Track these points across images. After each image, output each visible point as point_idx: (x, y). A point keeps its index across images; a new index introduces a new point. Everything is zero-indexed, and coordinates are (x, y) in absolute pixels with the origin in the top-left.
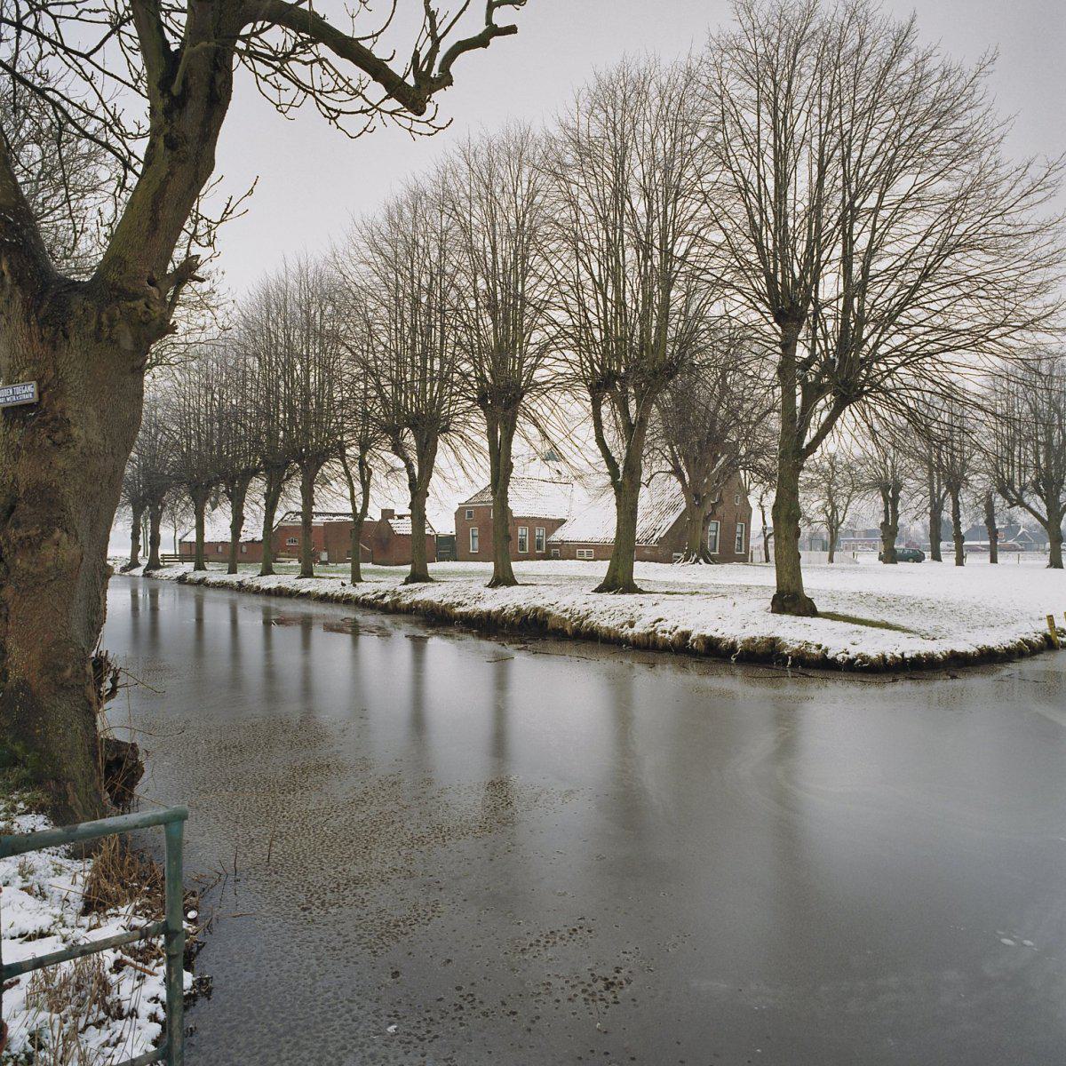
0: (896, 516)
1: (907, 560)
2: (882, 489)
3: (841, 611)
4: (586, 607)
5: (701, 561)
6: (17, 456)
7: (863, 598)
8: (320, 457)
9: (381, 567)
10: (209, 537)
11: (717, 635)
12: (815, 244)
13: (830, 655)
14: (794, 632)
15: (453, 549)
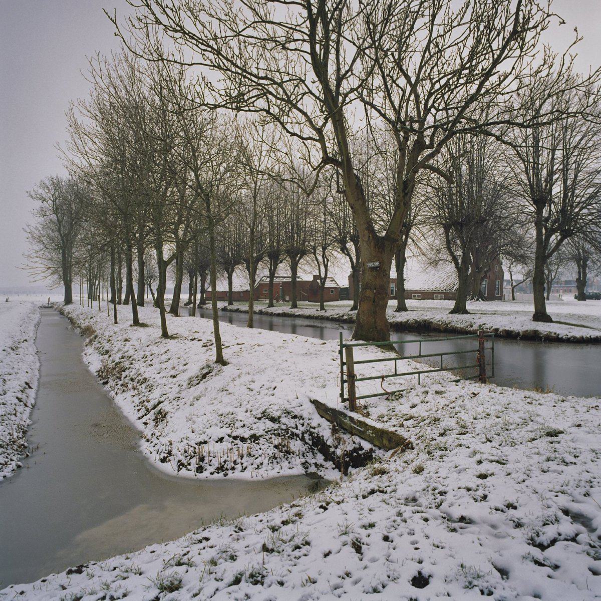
0: (585, 274)
1: (592, 299)
2: (576, 260)
3: (562, 320)
4: (449, 319)
5: (480, 300)
6: (376, 279)
7: (572, 316)
8: (303, 253)
9: (314, 303)
10: (235, 289)
11: (511, 329)
12: (551, 174)
13: (560, 336)
14: (543, 328)
15: (348, 294)
